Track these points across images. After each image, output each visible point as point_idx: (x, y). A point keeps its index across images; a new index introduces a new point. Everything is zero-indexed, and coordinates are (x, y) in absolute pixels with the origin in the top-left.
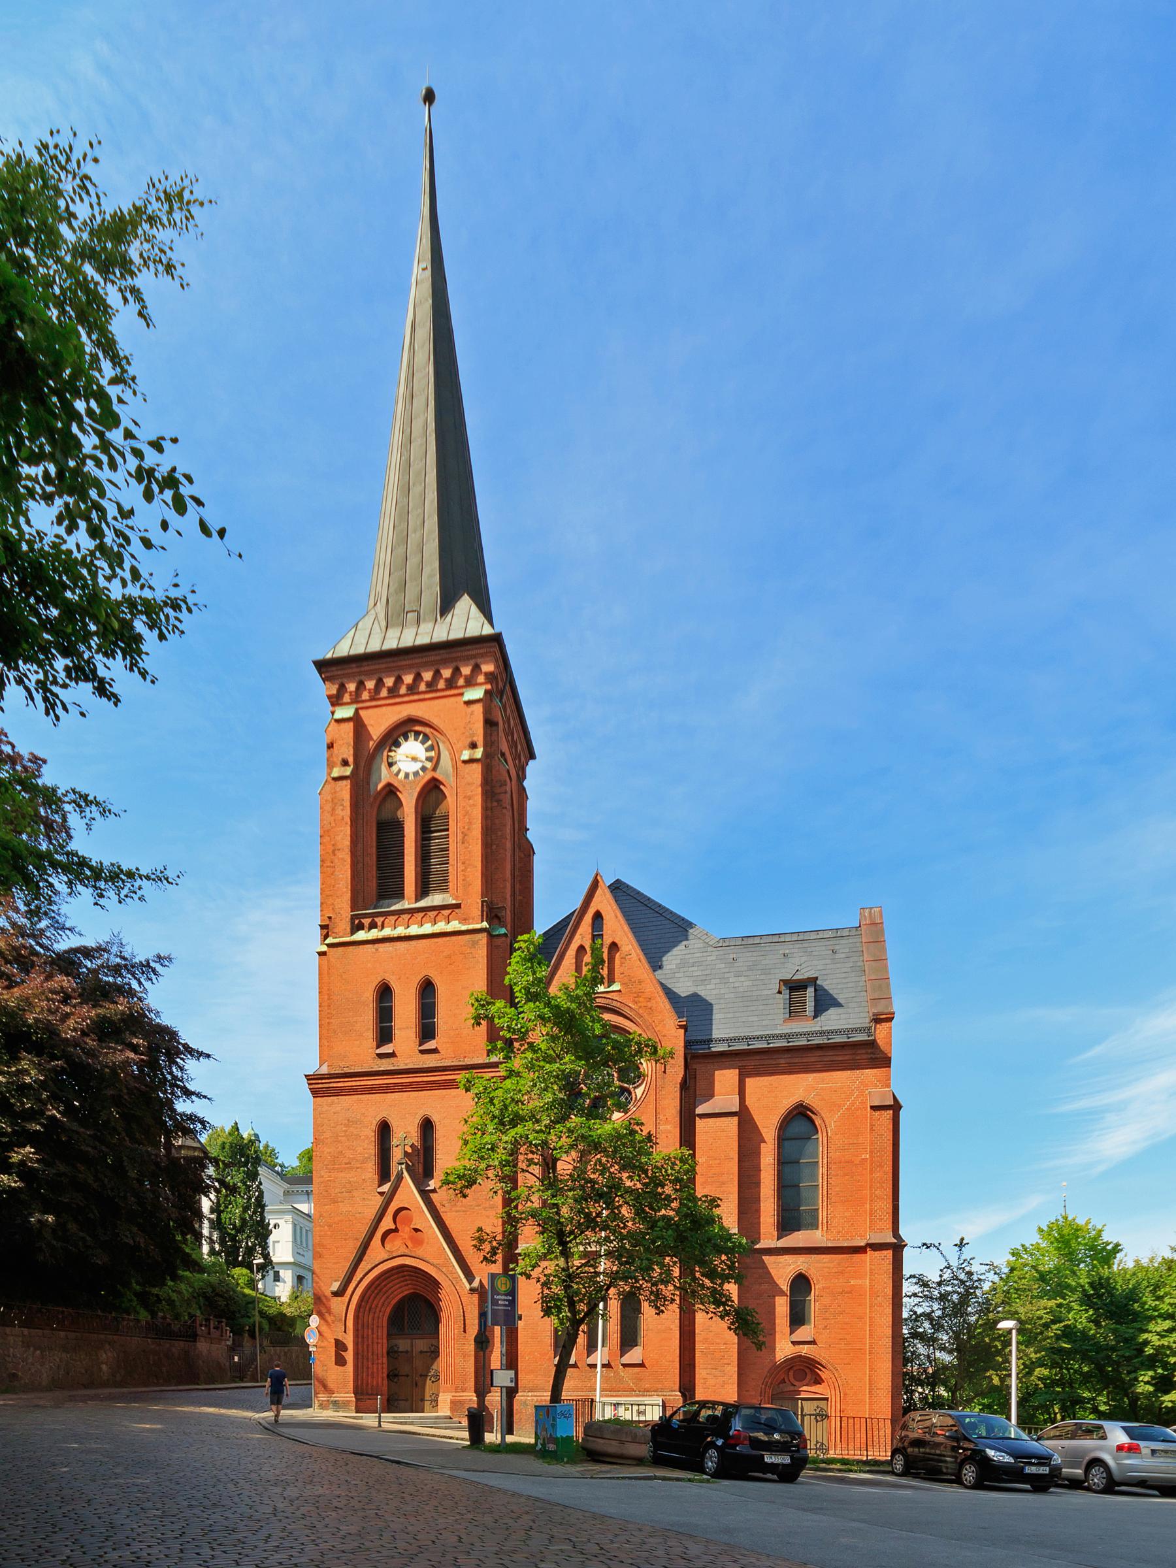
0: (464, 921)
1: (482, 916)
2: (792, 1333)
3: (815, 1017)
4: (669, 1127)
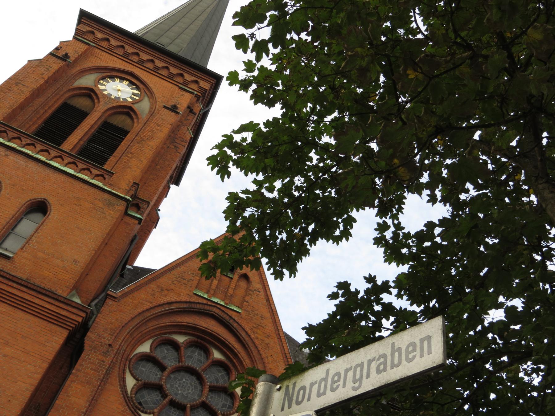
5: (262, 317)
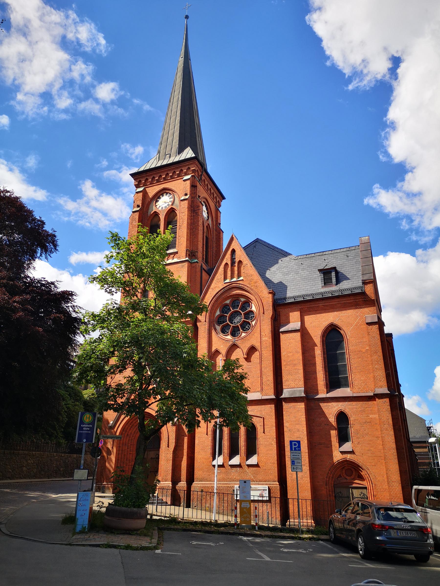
0: (179, 258)
1: (186, 255)
2: (340, 446)
3: (336, 284)
4: (266, 338)
5: (252, 275)
